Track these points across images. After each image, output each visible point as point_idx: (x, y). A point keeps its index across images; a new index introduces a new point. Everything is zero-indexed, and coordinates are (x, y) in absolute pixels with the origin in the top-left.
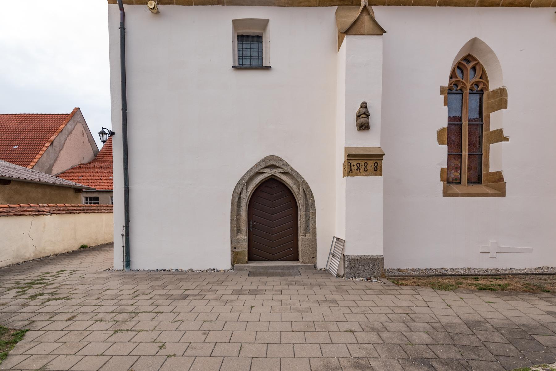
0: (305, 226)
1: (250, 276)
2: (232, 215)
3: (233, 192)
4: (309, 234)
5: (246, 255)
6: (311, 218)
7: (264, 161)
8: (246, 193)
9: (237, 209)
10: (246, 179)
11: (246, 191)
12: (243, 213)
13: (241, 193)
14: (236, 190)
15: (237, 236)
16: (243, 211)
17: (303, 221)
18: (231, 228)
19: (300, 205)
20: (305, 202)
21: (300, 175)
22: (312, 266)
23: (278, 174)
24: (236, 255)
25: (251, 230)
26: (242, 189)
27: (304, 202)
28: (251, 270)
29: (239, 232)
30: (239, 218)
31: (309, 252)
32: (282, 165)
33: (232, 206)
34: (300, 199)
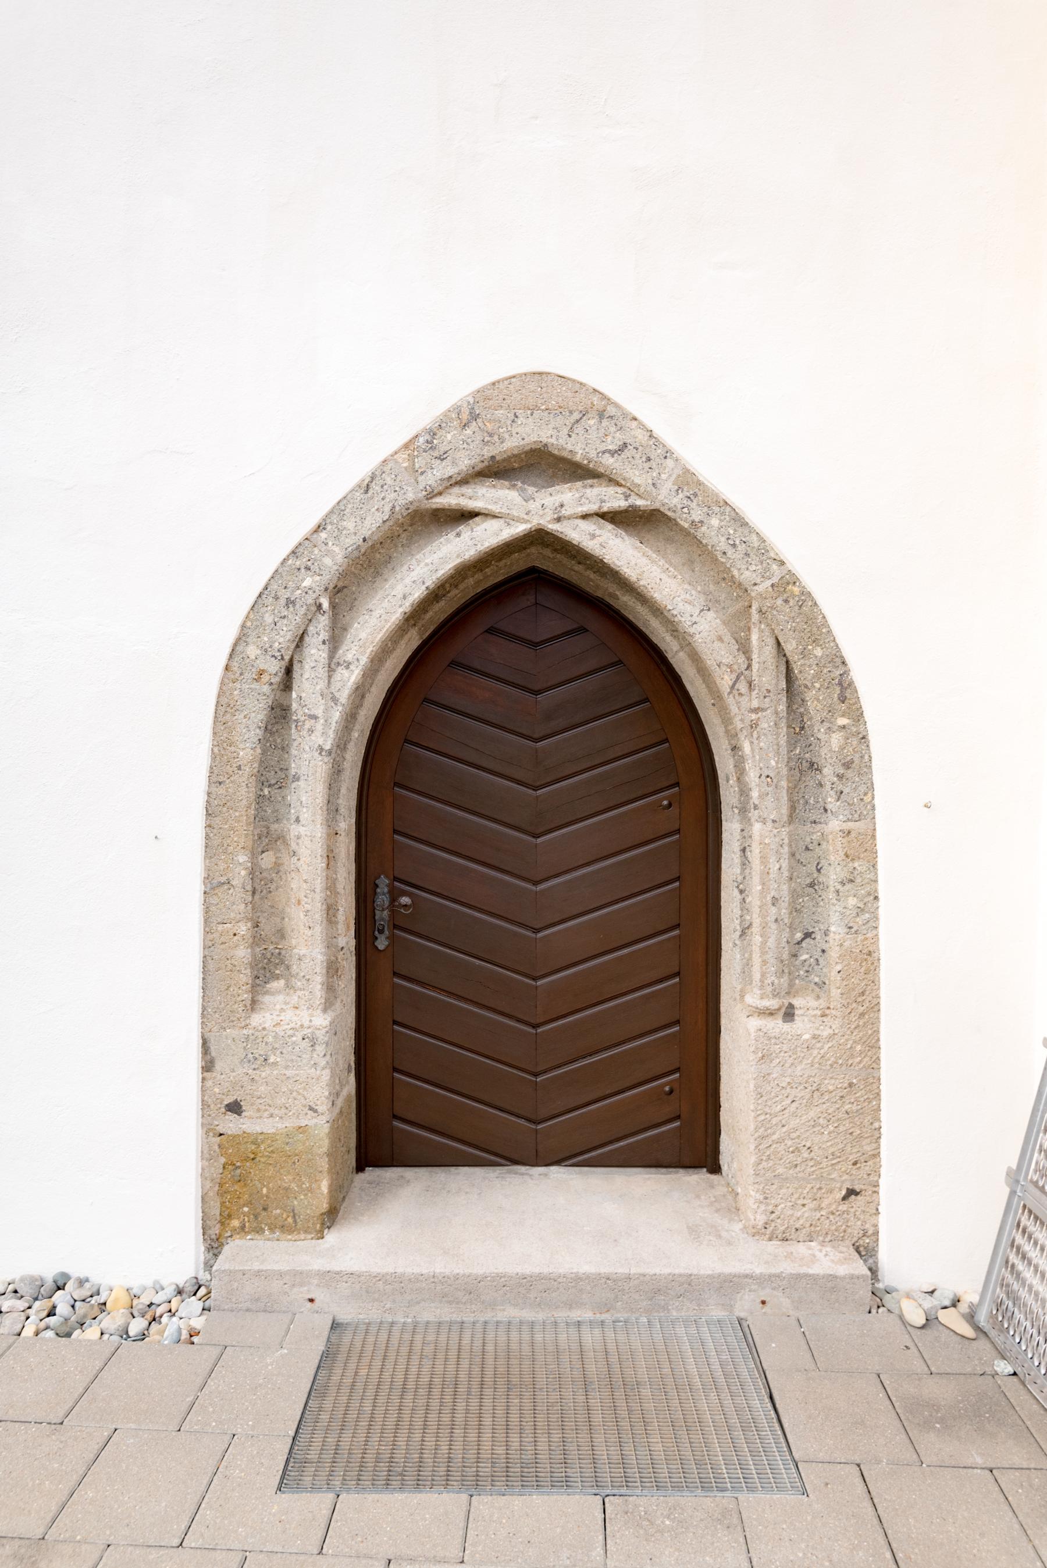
0: (786, 935)
1: (298, 1487)
2: (213, 848)
3: (227, 668)
4: (813, 1003)
5: (324, 1164)
6: (833, 875)
7: (474, 417)
8: (331, 670)
9: (260, 798)
10: (328, 561)
11: (331, 657)
12: (302, 830)
13: (289, 671)
14: (252, 651)
15: (254, 1005)
16: (305, 815)
17: (775, 901)
18: (208, 946)
19: (752, 776)
20: (792, 745)
21: (752, 531)
22: (852, 1277)
23: (583, 525)
24: (247, 1159)
25: (382, 943)
26: (300, 641)
27: (784, 751)
28: (347, 1314)
29: (277, 977)
30: (277, 867)
31: (817, 1152)
32: (613, 453)
33: (215, 780)
34: (754, 726)
